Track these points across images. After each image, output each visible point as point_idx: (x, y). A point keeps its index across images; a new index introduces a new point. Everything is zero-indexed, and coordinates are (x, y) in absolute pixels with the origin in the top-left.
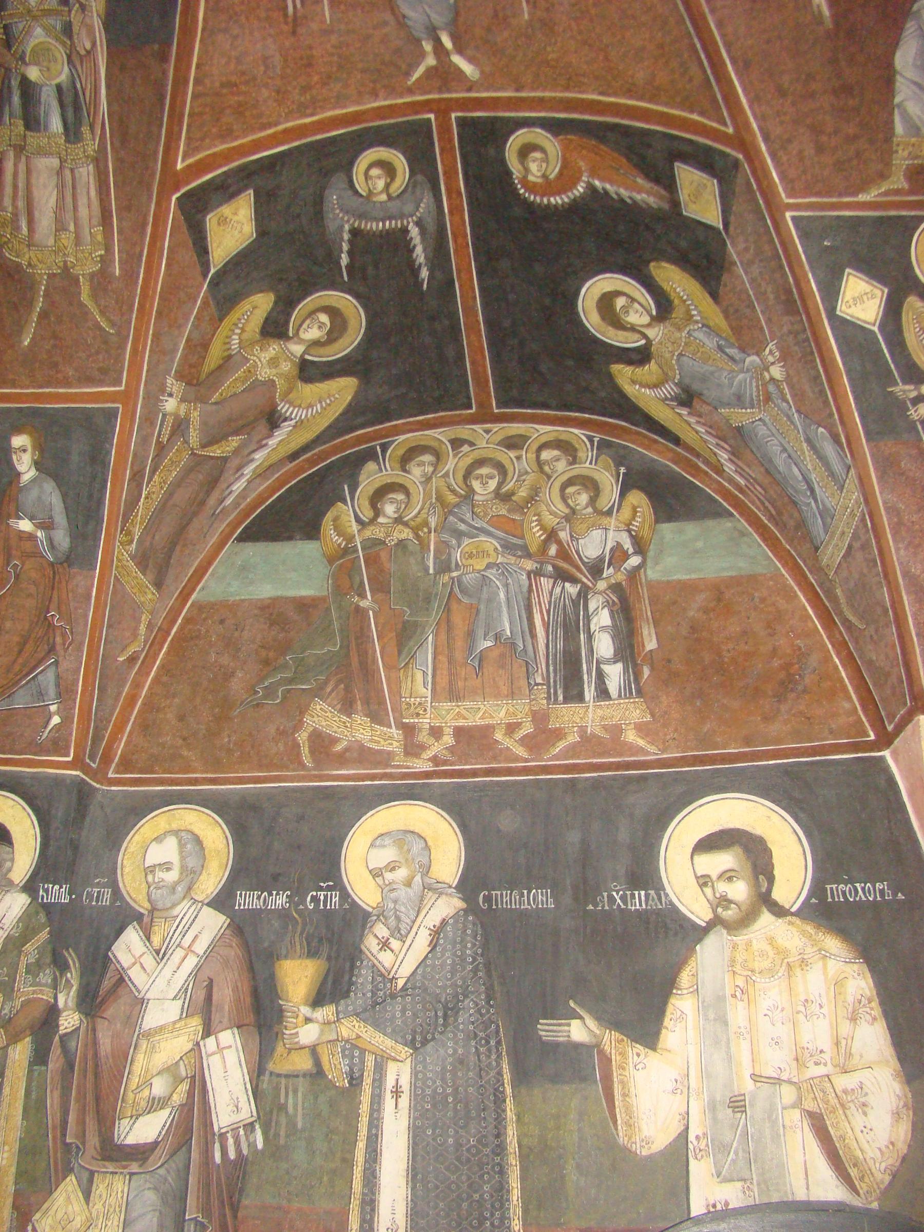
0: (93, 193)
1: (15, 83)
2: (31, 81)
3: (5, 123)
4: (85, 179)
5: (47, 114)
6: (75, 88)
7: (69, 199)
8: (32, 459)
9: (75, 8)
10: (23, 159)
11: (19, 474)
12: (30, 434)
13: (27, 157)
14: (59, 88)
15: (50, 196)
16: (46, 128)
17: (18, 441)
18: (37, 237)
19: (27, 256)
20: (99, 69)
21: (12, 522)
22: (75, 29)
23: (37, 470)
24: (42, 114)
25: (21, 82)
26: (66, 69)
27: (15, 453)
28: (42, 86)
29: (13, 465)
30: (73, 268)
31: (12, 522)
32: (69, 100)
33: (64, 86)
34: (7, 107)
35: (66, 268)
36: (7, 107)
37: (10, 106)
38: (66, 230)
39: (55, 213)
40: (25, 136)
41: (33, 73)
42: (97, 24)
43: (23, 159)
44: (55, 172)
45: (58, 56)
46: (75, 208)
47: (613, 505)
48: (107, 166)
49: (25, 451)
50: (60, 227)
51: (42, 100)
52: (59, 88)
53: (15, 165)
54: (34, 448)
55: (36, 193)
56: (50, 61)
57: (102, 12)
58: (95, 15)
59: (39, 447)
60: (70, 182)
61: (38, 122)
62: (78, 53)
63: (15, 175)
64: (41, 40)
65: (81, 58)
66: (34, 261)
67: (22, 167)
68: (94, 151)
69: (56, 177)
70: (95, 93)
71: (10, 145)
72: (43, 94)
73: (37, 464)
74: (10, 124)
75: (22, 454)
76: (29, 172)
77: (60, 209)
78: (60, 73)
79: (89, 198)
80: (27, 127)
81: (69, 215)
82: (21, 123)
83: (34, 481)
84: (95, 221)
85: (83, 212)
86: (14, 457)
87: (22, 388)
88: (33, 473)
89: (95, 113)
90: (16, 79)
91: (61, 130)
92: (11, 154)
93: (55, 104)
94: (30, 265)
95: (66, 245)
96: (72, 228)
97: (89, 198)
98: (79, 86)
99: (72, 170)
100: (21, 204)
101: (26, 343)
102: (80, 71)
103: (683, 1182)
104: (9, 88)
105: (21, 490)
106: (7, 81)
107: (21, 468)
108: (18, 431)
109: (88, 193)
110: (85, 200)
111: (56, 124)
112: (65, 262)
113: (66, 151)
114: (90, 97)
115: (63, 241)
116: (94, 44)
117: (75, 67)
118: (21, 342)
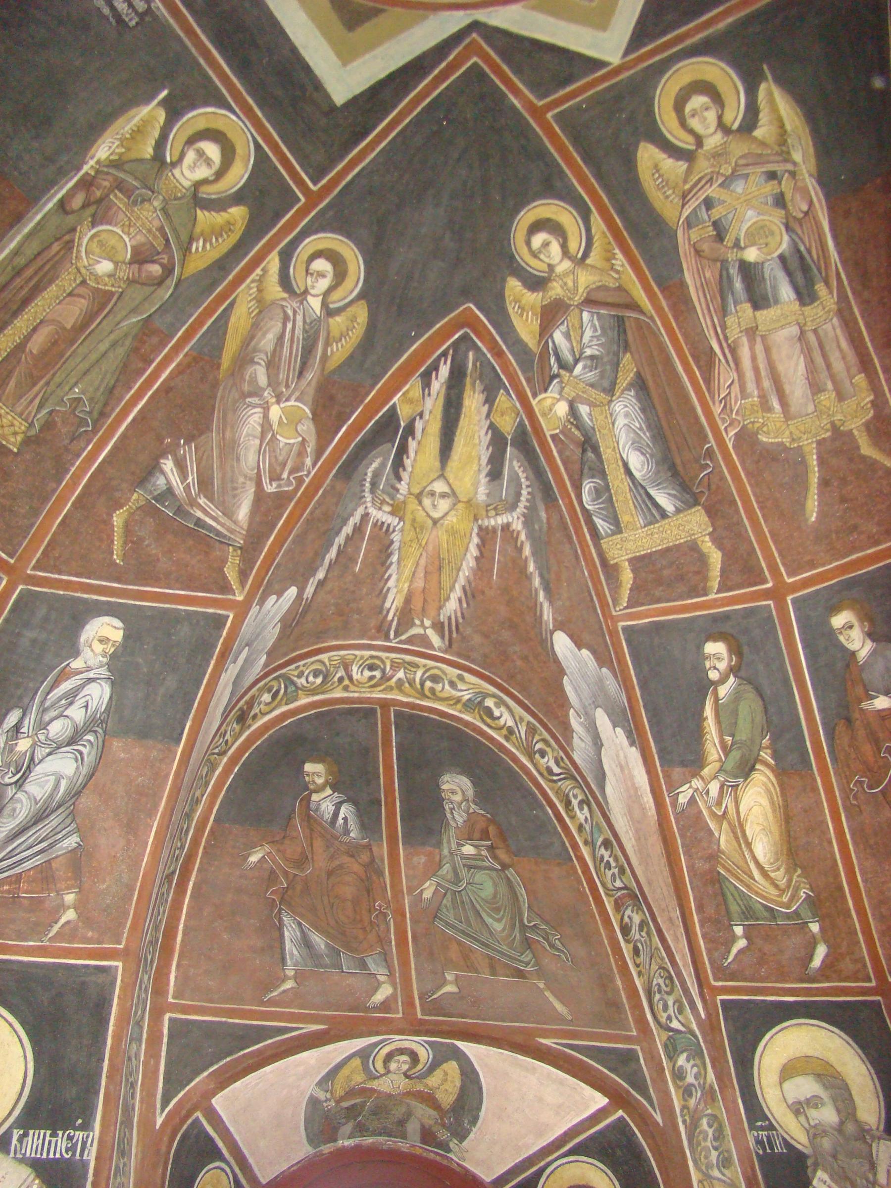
0: (844, 344)
1: (734, 271)
2: (750, 263)
3: (731, 313)
4: (831, 334)
5: (775, 288)
6: (799, 251)
7: (819, 360)
8: (863, 631)
9: (785, 178)
10: (758, 339)
11: (853, 654)
12: (851, 608)
13: (762, 336)
14: (782, 258)
15: (797, 365)
16: (777, 302)
17: (838, 621)
18: (793, 409)
19: (787, 433)
20: (821, 224)
21: (865, 705)
22: (788, 197)
23: (873, 640)
24: (769, 290)
25: (740, 267)
26: (786, 238)
27: (841, 633)
28: (763, 263)
29: (843, 646)
30: (843, 425)
31: (865, 705)
32: (794, 264)
33: (787, 254)
34: (730, 296)
35: (834, 428)
36: (730, 296)
37: (733, 294)
38: (824, 390)
39: (808, 379)
40: (755, 316)
41: (752, 255)
42: (811, 184)
43: (758, 339)
44: (796, 339)
45: (775, 228)
46: (829, 366)
47: (258, 147)
48: (852, 313)
49: (851, 627)
50: (815, 388)
51: (767, 276)
52: (782, 258)
53: (752, 349)
54: (861, 620)
55: (781, 368)
56: (767, 237)
57: (813, 169)
58: (807, 176)
59: (865, 616)
60: (816, 344)
61: (765, 298)
62: (794, 218)
63: (754, 358)
64: (754, 220)
65: (800, 222)
66: (797, 433)
67: (759, 347)
68: (834, 303)
69: (798, 345)
70: (823, 250)
71: (741, 332)
72: (765, 270)
73: (871, 635)
74: (737, 312)
75: (848, 632)
76: (767, 350)
77: (812, 372)
78: (780, 244)
79: (841, 350)
80: (756, 307)
81: (824, 375)
82: (747, 307)
83: (873, 653)
84: (854, 370)
85: (838, 366)
86: (841, 638)
87: (823, 565)
88: (869, 645)
89: (826, 266)
90: (733, 267)
91: (792, 295)
92: (745, 340)
93: (781, 276)
94: (793, 440)
95: (828, 405)
96: (830, 386)
97: (841, 350)
98: (802, 248)
99: (815, 331)
100: (767, 384)
101: (813, 519)
102: (800, 232)
103: (179, 731)
104: (729, 277)
105: (862, 668)
106: (724, 273)
107: (852, 647)
108: (835, 609)
109: (839, 346)
110: (837, 354)
111: (786, 292)
112: (833, 424)
113: (803, 314)
114: (818, 254)
115: (824, 403)
116: (811, 204)
117: (793, 231)
118: (807, 520)
